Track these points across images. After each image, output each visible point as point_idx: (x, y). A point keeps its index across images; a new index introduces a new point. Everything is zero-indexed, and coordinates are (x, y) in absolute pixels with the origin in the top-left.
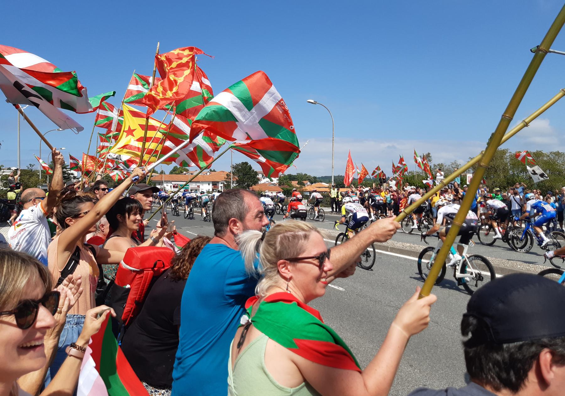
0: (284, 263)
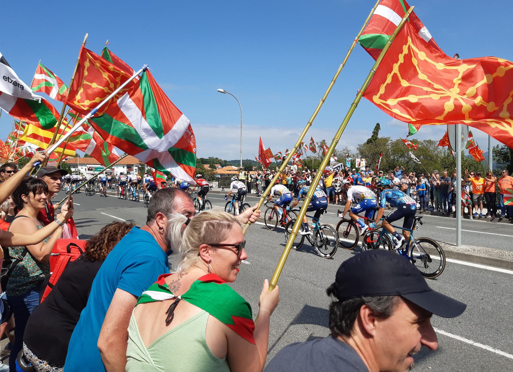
0: (206, 247)
